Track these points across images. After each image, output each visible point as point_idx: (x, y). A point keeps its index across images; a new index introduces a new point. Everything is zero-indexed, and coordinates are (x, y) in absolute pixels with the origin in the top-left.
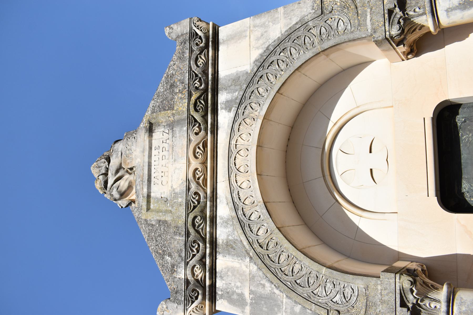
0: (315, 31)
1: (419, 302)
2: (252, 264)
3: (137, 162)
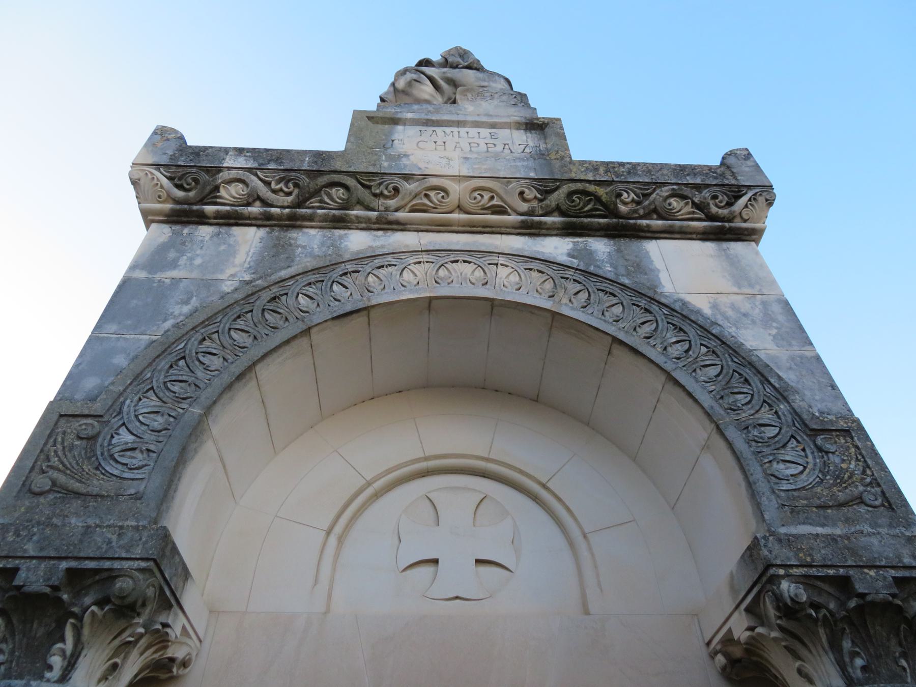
0: (765, 416)
1: (72, 620)
2: (236, 284)
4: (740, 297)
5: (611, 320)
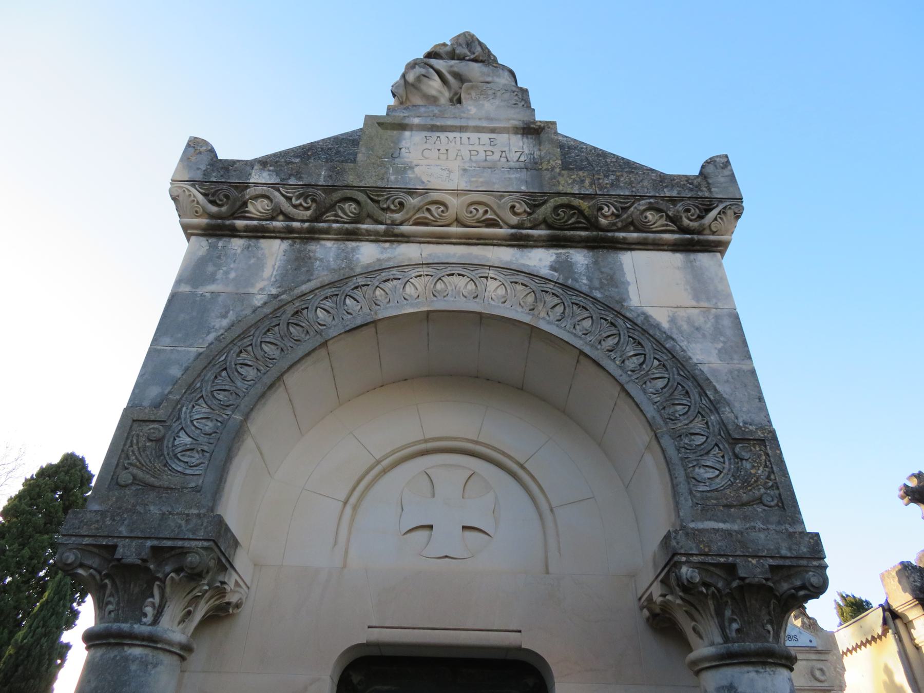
0: (698, 425)
1: (157, 583)
3: (469, 108)
4: (696, 311)
5: (580, 334)
